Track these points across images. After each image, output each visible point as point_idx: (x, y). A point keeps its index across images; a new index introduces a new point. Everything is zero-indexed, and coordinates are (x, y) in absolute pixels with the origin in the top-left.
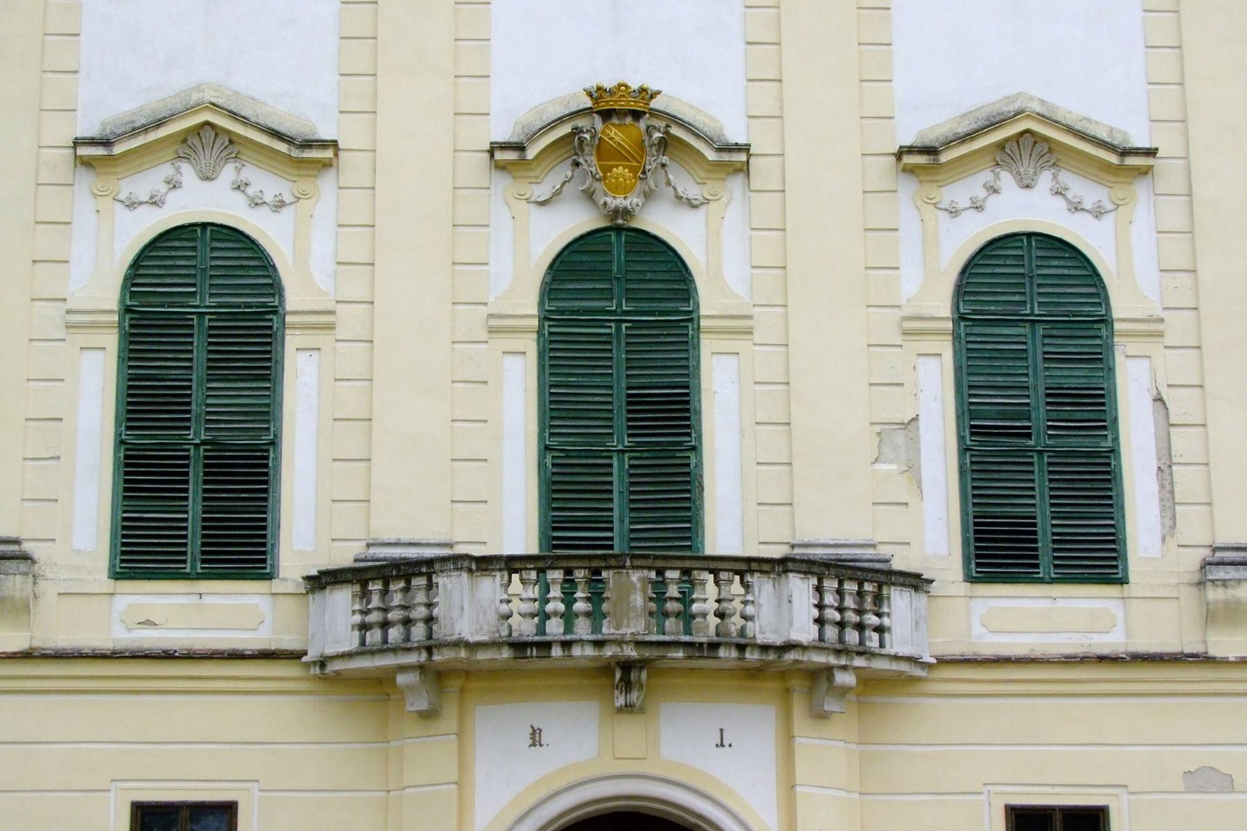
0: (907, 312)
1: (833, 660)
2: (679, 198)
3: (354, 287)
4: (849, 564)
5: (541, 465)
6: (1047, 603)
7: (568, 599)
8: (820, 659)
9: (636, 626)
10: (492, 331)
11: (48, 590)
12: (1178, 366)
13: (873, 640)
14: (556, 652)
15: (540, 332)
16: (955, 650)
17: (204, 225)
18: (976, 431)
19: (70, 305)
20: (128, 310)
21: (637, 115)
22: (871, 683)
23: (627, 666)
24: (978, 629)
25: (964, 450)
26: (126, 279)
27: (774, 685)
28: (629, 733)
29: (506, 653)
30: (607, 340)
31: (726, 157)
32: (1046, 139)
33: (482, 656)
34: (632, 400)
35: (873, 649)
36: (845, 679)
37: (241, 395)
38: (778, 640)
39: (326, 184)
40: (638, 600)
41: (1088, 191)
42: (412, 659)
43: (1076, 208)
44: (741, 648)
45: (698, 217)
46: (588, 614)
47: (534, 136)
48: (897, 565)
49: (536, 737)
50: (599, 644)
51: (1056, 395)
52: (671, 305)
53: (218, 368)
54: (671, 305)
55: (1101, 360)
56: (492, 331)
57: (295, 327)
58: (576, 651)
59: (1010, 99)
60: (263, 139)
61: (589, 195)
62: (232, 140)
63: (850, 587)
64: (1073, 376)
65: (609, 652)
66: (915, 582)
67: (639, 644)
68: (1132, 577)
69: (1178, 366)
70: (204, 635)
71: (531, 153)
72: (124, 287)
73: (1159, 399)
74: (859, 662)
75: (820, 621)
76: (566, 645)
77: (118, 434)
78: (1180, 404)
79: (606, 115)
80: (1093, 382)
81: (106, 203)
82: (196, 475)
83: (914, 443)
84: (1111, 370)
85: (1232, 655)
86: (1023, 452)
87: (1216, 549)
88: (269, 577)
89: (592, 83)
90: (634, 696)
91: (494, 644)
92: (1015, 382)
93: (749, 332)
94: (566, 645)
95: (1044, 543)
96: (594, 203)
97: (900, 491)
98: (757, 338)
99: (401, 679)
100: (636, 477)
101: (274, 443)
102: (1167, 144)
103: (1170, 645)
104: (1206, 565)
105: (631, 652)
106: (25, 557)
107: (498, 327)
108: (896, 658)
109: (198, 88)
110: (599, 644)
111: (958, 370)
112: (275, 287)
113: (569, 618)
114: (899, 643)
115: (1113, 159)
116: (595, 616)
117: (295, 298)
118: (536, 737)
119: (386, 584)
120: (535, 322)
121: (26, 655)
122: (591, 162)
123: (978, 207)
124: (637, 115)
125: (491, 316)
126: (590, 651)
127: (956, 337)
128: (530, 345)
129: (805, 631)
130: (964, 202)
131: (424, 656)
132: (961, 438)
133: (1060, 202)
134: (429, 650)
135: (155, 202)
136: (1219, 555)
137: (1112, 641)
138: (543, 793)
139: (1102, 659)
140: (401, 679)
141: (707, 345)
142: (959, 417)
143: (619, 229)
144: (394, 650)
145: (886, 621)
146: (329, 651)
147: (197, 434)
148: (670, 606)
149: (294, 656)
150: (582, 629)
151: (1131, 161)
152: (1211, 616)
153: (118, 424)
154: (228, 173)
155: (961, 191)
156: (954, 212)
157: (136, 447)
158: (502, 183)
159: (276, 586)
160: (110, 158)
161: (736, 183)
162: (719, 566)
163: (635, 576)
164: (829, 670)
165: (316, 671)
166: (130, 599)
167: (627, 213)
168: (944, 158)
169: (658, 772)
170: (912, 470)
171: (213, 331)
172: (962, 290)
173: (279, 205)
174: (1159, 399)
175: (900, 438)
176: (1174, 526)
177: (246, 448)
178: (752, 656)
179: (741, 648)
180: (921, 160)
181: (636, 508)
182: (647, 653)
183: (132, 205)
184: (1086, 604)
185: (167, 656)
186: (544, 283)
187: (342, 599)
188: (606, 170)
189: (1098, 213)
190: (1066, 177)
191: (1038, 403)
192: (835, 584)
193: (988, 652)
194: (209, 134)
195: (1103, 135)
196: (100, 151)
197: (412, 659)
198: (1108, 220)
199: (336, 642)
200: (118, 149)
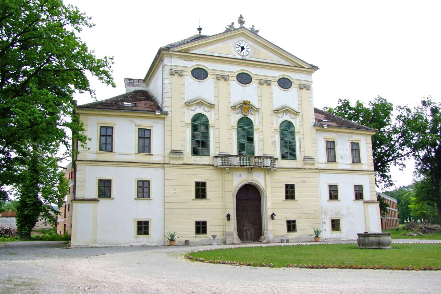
0: (275, 129)
2: (251, 114)
3: (217, 122)
5: (238, 144)
6: (289, 162)
7: (243, 160)
8: (270, 168)
9: (253, 164)
10: (232, 128)
11: (185, 157)
12: (301, 136)
14: (245, 166)
15: (237, 129)
16: (280, 167)
17: (200, 114)
18: (282, 143)
19: (185, 122)
20: (192, 123)
21: (248, 104)
22: (274, 170)
23: (251, 168)
24: (282, 165)
25: (281, 145)
26: (192, 119)
27: (264, 170)
28: (250, 175)
29: (240, 166)
30: (244, 130)
31: (257, 110)
32: (289, 110)
33: (237, 166)
34: (247, 137)
36: (272, 170)
38: (267, 166)
39: (213, 110)
41: (293, 116)
42: (229, 166)
43: (291, 118)
44: (263, 166)
45: (253, 116)
46: (248, 162)
47: (237, 106)
49: (240, 176)
50: (250, 166)
51: (290, 139)
52: (251, 126)
53: (203, 131)
54: (251, 126)
55: (294, 135)
56: (232, 128)
57: (211, 126)
58: (247, 166)
59: (285, 105)
60: (207, 104)
61: (242, 113)
62: (203, 103)
63: (273, 160)
64: (291, 137)
65: (251, 167)
66: (277, 159)
67: (254, 166)
68: (297, 159)
69: (301, 136)
70: (202, 162)
71: (236, 108)
72: (191, 120)
73: (299, 140)
74: (273, 168)
76: (246, 166)
77: (192, 138)
78: (302, 140)
79: (245, 104)
80: (293, 138)
81: (189, 110)
82: (200, 143)
83: (276, 143)
84: (295, 136)
85: (307, 168)
86: (287, 145)
87: (305, 157)
88: (209, 156)
90: (251, 171)
91: (239, 165)
93: (259, 130)
94: (246, 166)
95: (289, 155)
96: (243, 114)
97: (274, 149)
98: (260, 131)
99: (227, 169)
100: (248, 146)
101: (209, 140)
102: (216, 103)
103: (300, 167)
104: (304, 158)
106: (183, 153)
107: (233, 128)
108: (276, 168)
109: (199, 97)
110: (250, 166)
111: (280, 135)
112: (208, 122)
113: (243, 162)
115: (296, 113)
116: (249, 163)
117: (210, 123)
118: (240, 176)
119: (13, 148)
120: (237, 128)
121: (183, 164)
122: (243, 109)
123: (282, 117)
124: (248, 104)
125: (232, 127)
126: (249, 166)
127: (280, 132)
128: (236, 130)
129: (269, 165)
131: (230, 166)
132: (280, 143)
133: (290, 117)
134: (231, 165)
135: (194, 110)
136: (220, 153)
137: (295, 166)
138: (241, 182)
139: (295, 168)
140: (227, 169)
141: (255, 131)
142: (280, 141)
143: (245, 117)
144: (226, 165)
145: (264, 162)
146: (218, 165)
147: (200, 139)
149: (213, 165)
150: (248, 164)
151: (297, 113)
152: (305, 164)
153: (191, 137)
154: (202, 107)
155: (280, 115)
156: (279, 118)
157: (194, 140)
158: (232, 111)
159: (210, 157)
160: (190, 105)
161: (257, 113)
162: (256, 157)
164: (270, 169)
165: (215, 167)
166: (194, 158)
167: (247, 115)
168: (279, 111)
169: (253, 180)
170: (276, 146)
173: (208, 112)
174: (299, 140)
175: (274, 143)
176: (301, 154)
177: (206, 141)
178: (264, 167)
179: (263, 166)
180: (277, 111)
181: (248, 150)
182: (254, 167)
183: (192, 111)
184: (292, 162)
185: (199, 165)
186: (237, 123)
187: (219, 160)
188: (245, 110)
189: (294, 119)
190: (205, 108)
191: (288, 139)
192: (242, 158)
193: (283, 167)
194: (200, 103)
196: (189, 104)
197: (229, 166)
198: (209, 113)
199: (219, 164)
200: (191, 104)
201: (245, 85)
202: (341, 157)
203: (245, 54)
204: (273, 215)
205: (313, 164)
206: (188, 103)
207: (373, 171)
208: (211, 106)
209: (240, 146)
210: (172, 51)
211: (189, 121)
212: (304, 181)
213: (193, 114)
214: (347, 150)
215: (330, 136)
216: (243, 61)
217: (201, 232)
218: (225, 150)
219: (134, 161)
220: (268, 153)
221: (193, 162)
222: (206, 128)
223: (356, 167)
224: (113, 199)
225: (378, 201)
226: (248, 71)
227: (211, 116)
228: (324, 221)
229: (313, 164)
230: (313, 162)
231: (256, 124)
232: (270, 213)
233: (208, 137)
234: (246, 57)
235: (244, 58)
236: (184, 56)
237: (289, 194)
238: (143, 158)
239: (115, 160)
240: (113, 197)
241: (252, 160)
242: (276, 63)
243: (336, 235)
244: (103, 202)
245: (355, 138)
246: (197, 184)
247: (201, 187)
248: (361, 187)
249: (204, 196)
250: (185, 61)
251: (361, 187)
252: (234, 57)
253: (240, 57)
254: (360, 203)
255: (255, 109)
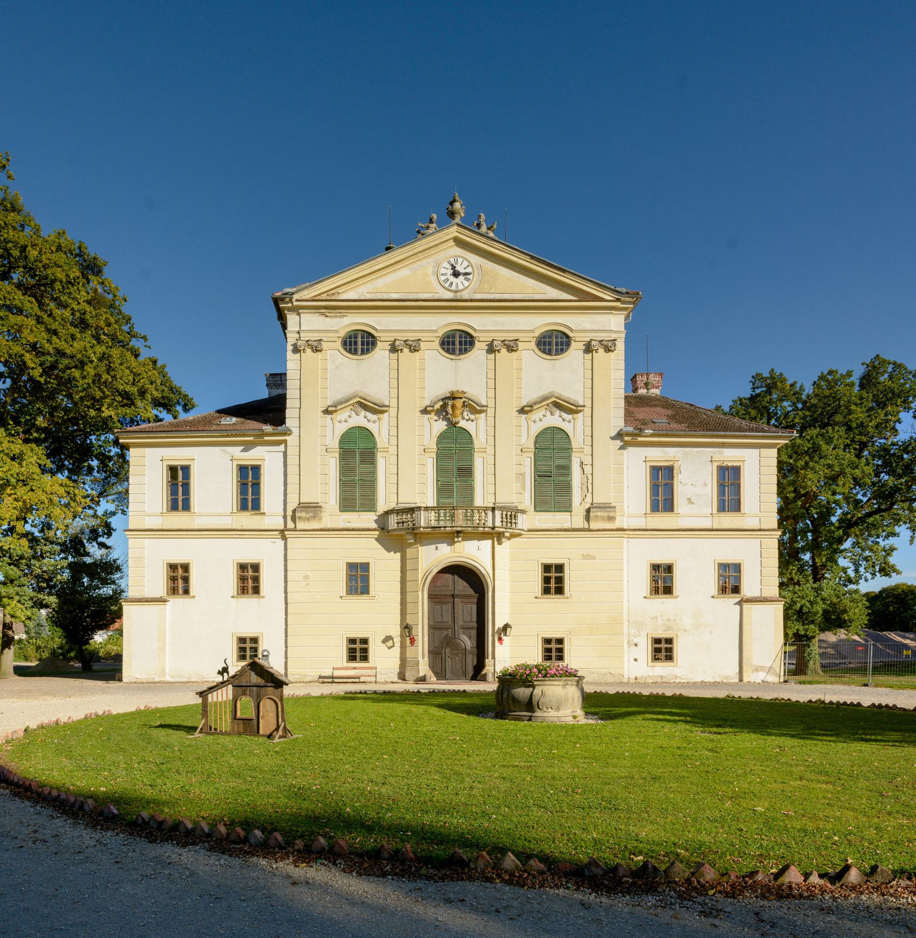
1: (504, 530)
4: (634, 709)
13: (514, 526)
35: (564, 719)
36: (507, 534)
37: (366, 468)
40: (461, 517)
48: (519, 508)
51: (559, 467)
53: (363, 462)
55: (471, 456)
65: (455, 529)
66: (523, 512)
75: (502, 522)
83: (524, 478)
89: (450, 390)
92: (355, 668)
105: (459, 529)
106: (321, 507)
114: (519, 526)
120: (436, 450)
121: (322, 530)
130: (538, 419)
135: (369, 421)
137: (567, 525)
148: (469, 518)
151: (579, 408)
162: (479, 509)
163: (460, 511)
164: (503, 532)
170: (523, 484)
171: (361, 454)
172: (536, 442)
175: (521, 477)
185: (353, 530)
193: (539, 528)
195: (572, 402)
201: (457, 358)
202: (687, 501)
203: (461, 287)
204: (506, 627)
205: (611, 519)
206: (332, 406)
207: (774, 530)
208: (380, 409)
209: (443, 490)
210: (297, 300)
211: (335, 444)
212: (587, 557)
213: (341, 429)
214: (706, 485)
215: (661, 455)
216: (456, 304)
217: (358, 658)
218: (408, 499)
219: (230, 527)
220: (504, 498)
221: (341, 525)
222: (369, 456)
223: (729, 520)
224: (194, 597)
225: (781, 599)
226: (460, 324)
227: (380, 428)
228: (635, 641)
229: (611, 519)
230: (611, 514)
231: (480, 440)
232: (499, 624)
233: (374, 473)
234: (463, 293)
235: (458, 296)
236: (326, 308)
237: (661, 584)
238: (247, 520)
239: (196, 527)
240: (677, 594)
241: (458, 514)
242: (535, 298)
243: (662, 670)
244: (177, 603)
245: (730, 456)
246: (351, 566)
247: (553, 575)
248: (737, 567)
249: (365, 590)
250: (327, 319)
251: (737, 567)
252: (437, 296)
253: (450, 295)
254: (731, 601)
255: (478, 408)
